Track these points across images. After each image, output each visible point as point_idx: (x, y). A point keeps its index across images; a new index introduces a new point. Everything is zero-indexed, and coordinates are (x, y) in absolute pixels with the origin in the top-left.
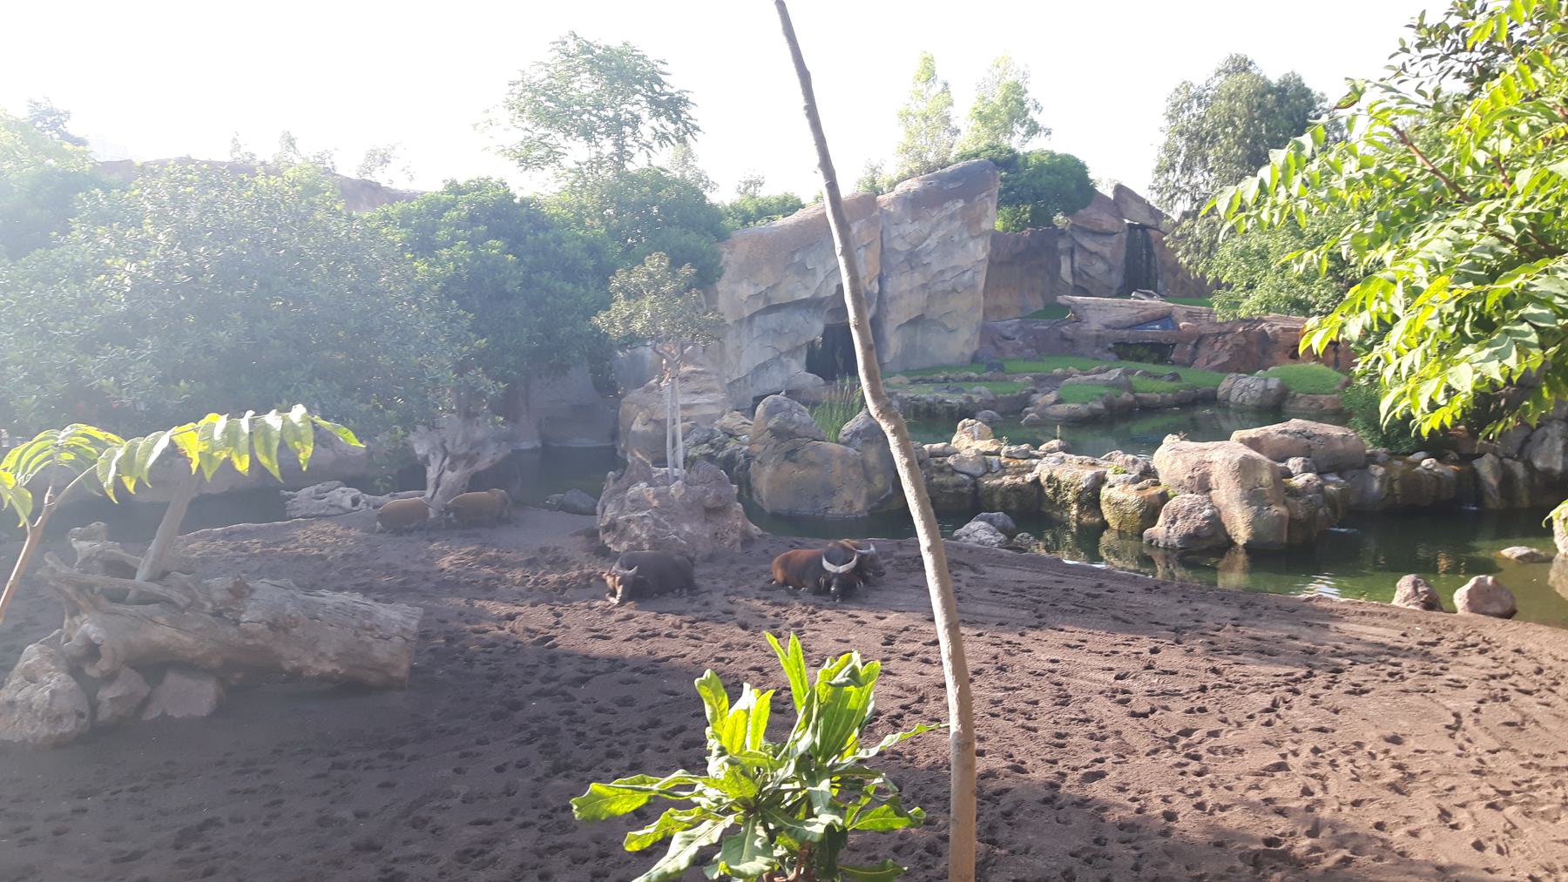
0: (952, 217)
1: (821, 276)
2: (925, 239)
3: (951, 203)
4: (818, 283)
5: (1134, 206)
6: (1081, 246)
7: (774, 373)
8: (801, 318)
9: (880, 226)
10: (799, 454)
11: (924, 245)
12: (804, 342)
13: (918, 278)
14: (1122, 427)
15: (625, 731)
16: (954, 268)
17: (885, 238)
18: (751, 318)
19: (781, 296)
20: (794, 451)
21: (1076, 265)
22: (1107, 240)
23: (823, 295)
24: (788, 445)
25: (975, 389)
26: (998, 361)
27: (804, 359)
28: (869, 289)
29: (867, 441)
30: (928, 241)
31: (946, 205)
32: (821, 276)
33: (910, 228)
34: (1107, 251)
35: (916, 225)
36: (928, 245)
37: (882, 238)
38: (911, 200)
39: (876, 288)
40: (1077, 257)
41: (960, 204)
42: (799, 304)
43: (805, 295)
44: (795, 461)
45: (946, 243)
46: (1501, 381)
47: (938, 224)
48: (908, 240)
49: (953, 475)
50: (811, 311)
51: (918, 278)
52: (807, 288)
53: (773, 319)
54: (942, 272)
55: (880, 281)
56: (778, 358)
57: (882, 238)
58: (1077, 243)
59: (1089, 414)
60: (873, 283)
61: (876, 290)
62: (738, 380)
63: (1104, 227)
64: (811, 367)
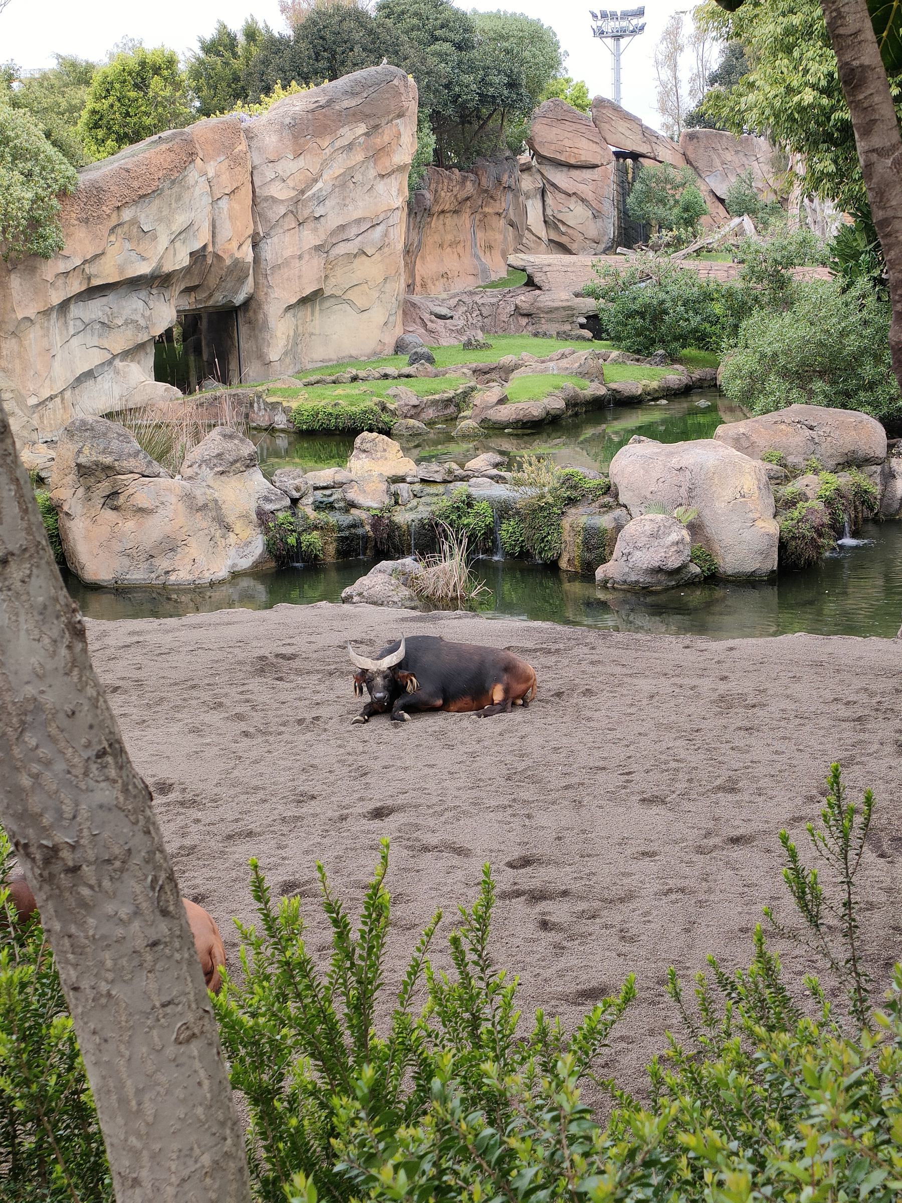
0: (350, 147)
1: (163, 241)
2: (316, 181)
3: (347, 128)
4: (161, 248)
5: (622, 126)
6: (553, 185)
7: (107, 386)
8: (141, 303)
9: (249, 163)
10: (121, 499)
11: (315, 189)
12: (146, 338)
13: (310, 237)
14: (589, 432)
15: (525, 770)
16: (358, 221)
17: (257, 183)
18: (64, 306)
19: (107, 273)
20: (114, 494)
21: (549, 212)
22: (587, 174)
23: (168, 268)
24: (104, 487)
25: (392, 391)
26: (425, 350)
27: (150, 361)
28: (238, 255)
29: (222, 473)
30: (320, 185)
31: (342, 131)
32: (163, 241)
33: (289, 166)
34: (586, 190)
35: (301, 162)
36: (321, 190)
37: (252, 183)
38: (291, 126)
39: (247, 254)
40: (549, 200)
41: (362, 129)
42: (135, 284)
43: (144, 269)
44: (116, 508)
45: (345, 181)
46: (293, 83)
47: (331, 158)
48: (291, 184)
49: (347, 511)
50: (154, 291)
51: (310, 237)
52: (144, 259)
53: (95, 309)
54: (342, 228)
55: (255, 246)
56: (110, 362)
57: (252, 183)
58: (549, 181)
59: (544, 415)
60: (244, 247)
61: (250, 258)
62: (51, 398)
63: (583, 158)
64: (161, 375)
